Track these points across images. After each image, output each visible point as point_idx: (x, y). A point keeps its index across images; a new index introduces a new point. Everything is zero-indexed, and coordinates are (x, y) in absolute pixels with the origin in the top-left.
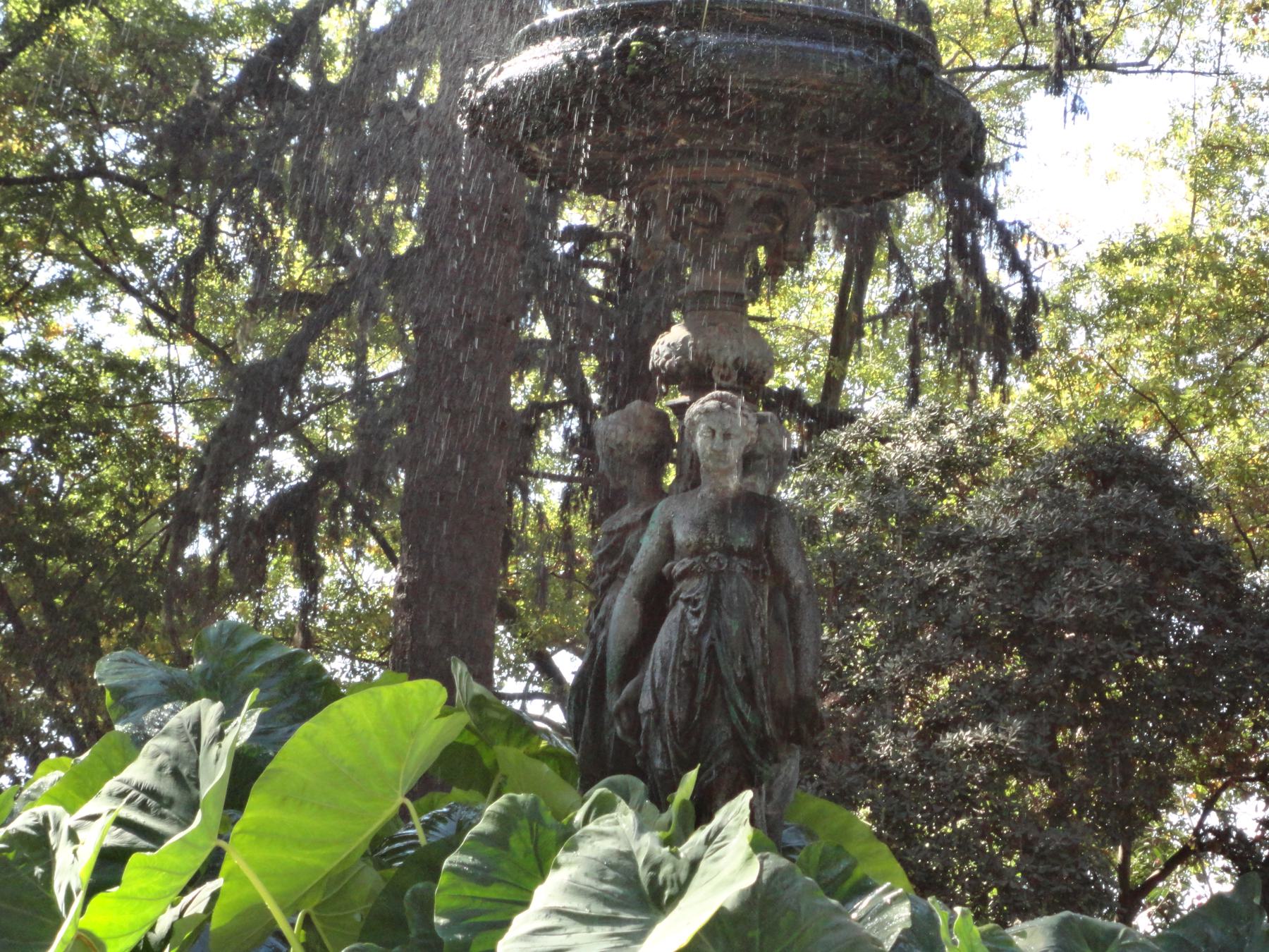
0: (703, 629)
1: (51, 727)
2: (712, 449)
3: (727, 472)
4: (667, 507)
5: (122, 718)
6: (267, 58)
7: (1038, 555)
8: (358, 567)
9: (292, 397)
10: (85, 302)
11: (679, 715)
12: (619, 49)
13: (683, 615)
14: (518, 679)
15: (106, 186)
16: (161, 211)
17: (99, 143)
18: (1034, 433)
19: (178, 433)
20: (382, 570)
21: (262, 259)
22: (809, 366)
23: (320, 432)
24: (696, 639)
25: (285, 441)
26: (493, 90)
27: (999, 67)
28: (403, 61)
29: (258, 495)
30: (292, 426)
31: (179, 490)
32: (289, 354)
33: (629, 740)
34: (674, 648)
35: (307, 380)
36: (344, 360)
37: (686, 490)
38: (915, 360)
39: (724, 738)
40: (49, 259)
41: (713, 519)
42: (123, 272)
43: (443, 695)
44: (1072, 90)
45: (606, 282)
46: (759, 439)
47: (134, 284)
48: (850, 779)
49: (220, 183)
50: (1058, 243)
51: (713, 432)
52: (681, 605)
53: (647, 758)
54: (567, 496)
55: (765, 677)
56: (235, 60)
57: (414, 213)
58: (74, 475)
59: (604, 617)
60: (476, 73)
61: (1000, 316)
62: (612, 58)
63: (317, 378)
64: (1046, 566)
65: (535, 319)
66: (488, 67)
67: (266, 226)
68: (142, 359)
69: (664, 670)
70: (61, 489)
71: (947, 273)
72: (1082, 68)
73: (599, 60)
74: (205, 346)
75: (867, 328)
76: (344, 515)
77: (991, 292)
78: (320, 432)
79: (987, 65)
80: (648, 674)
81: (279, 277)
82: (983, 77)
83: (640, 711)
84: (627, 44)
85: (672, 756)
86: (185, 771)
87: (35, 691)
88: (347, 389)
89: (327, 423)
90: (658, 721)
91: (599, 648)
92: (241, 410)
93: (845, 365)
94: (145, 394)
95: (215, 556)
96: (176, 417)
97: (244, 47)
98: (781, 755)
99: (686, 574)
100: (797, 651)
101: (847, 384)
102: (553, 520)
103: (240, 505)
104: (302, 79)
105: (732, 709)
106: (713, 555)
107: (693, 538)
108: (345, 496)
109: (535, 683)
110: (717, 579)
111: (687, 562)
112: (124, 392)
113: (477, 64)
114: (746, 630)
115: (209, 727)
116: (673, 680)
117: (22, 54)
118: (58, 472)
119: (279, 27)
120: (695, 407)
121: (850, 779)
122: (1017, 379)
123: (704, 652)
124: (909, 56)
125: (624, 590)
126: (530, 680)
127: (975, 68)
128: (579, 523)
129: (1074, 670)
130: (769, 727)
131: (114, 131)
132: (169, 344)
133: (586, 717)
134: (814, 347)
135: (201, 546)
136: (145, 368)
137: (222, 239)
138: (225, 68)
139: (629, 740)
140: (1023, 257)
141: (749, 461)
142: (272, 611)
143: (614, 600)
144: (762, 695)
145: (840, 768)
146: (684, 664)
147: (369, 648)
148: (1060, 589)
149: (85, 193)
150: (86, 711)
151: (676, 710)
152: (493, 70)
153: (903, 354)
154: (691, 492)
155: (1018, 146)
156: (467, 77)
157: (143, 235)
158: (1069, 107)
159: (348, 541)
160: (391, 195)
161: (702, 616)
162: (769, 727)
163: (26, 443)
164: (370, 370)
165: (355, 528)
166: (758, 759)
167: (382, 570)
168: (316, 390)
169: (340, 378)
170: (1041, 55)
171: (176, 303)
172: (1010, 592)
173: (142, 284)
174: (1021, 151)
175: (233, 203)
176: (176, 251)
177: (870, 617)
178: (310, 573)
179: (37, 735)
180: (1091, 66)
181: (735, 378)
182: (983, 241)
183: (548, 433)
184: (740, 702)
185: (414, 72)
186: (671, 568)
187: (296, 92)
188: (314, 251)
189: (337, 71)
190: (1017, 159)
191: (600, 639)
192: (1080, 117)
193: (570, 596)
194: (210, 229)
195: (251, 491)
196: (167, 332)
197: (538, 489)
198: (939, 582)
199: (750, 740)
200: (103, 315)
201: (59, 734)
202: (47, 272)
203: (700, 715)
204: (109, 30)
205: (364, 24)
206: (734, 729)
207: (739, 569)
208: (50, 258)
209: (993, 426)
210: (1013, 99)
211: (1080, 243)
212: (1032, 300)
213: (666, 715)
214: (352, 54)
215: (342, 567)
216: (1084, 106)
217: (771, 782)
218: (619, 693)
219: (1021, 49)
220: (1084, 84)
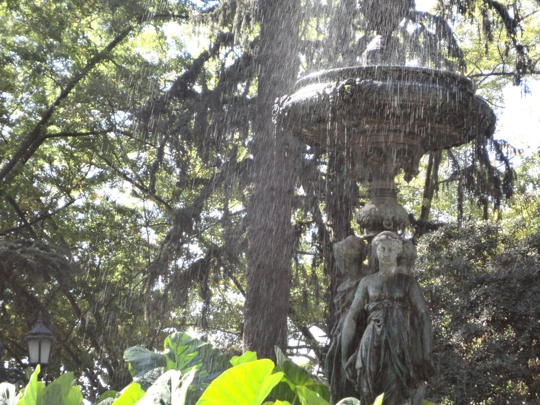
0: (382, 332)
1: (98, 364)
2: (384, 256)
3: (391, 265)
4: (365, 280)
5: (136, 375)
6: (183, 80)
7: (518, 285)
8: (226, 293)
9: (197, 223)
10: (108, 184)
11: (373, 369)
12: (340, 89)
13: (374, 326)
14: (295, 338)
15: (116, 136)
16: (140, 145)
17: (113, 117)
18: (514, 232)
19: (148, 238)
20: (236, 294)
21: (183, 164)
22: (415, 203)
23: (209, 236)
24: (379, 337)
25: (194, 241)
26: (287, 107)
27: (492, 74)
28: (240, 79)
29: (184, 264)
30: (198, 234)
31: (149, 263)
32: (195, 205)
33: (352, 381)
34: (370, 341)
35: (203, 215)
36: (218, 206)
37: (373, 273)
38: (460, 200)
39: (393, 378)
40: (93, 167)
41: (385, 285)
42: (124, 171)
43: (272, 364)
44: (524, 82)
45: (328, 170)
46: (403, 251)
47: (129, 176)
48: (441, 383)
49: (164, 133)
50: (520, 148)
51: (384, 249)
52: (372, 322)
53: (360, 388)
54: (314, 260)
55: (409, 351)
56: (169, 81)
57: (246, 143)
58: (106, 258)
59: (340, 328)
60: (279, 100)
61: (496, 181)
62: (337, 92)
63: (207, 214)
64: (521, 290)
65: (299, 187)
66: (285, 97)
67: (185, 152)
68: (133, 207)
69: (366, 350)
70: (100, 263)
71: (473, 162)
72: (528, 73)
73: (331, 94)
74: (159, 200)
75: (441, 186)
76: (220, 271)
77: (491, 170)
78: (209, 236)
79: (487, 73)
80: (359, 352)
81: (190, 172)
82: (486, 78)
83: (357, 368)
84: (343, 87)
85: (371, 387)
86: (165, 401)
87: (91, 349)
88: (220, 218)
89: (212, 233)
90: (364, 372)
91: (338, 341)
92: (175, 229)
93: (430, 202)
94: (134, 222)
95: (166, 291)
96: (147, 231)
97: (173, 76)
98: (417, 385)
99: (375, 309)
100: (422, 340)
101: (431, 210)
102: (309, 272)
103: (176, 267)
104: (198, 88)
105: (395, 366)
106: (385, 301)
107: (377, 294)
108: (220, 264)
109: (302, 341)
110: (388, 311)
111: (375, 304)
112: (126, 222)
113: (280, 96)
114: (400, 333)
115: (175, 383)
116: (370, 354)
117: (80, 81)
118: (99, 256)
119: (187, 66)
120: (376, 238)
121: (441, 383)
122: (504, 206)
123: (383, 342)
124: (463, 88)
125: (348, 316)
126: (300, 339)
127: (482, 75)
128: (319, 272)
129: (535, 334)
130: (412, 373)
131: (119, 112)
132: (144, 201)
133: (333, 371)
134: (417, 195)
135: (160, 285)
136: (133, 212)
137: (166, 157)
138: (165, 84)
139: (352, 381)
140: (505, 155)
141: (399, 260)
142: (190, 312)
143: (344, 321)
144: (408, 360)
145: (436, 379)
146: (375, 348)
147: (232, 327)
148: (529, 300)
149: (107, 138)
150: (113, 357)
151: (371, 368)
152: (286, 99)
153: (455, 197)
154: (375, 274)
155: (502, 107)
156: (276, 101)
157: (132, 156)
158: (523, 91)
159: (222, 282)
160: (237, 136)
161: (382, 327)
162: (412, 373)
163: (85, 245)
164: (230, 210)
165: (224, 276)
166: (407, 387)
167: (236, 294)
168: (207, 219)
169: (216, 214)
170: (510, 68)
171: (147, 184)
172: (507, 302)
173: (132, 176)
174: (503, 110)
175: (171, 141)
176: (146, 162)
177: (447, 314)
178: (206, 295)
179: (92, 368)
180: (532, 72)
181: (392, 225)
182: (488, 147)
183: (305, 235)
184: (399, 363)
185: (245, 84)
186: (368, 306)
187: (193, 94)
188: (205, 159)
189: (212, 85)
190: (502, 113)
191: (338, 337)
192: (528, 94)
193: (317, 303)
194: (161, 153)
195: (180, 262)
196: (143, 196)
197: (301, 258)
198: (476, 298)
199: (404, 380)
200: (116, 190)
201: (102, 367)
202: (93, 172)
203: (382, 369)
204: (116, 70)
205: (223, 65)
206: (397, 375)
207: (397, 307)
208: (93, 166)
209: (497, 230)
210: (498, 87)
211: (529, 147)
212: (510, 175)
213: (368, 369)
214: (218, 77)
215: (219, 293)
216: (529, 90)
217: (413, 397)
218: (347, 360)
219: (502, 66)
220: (529, 80)
